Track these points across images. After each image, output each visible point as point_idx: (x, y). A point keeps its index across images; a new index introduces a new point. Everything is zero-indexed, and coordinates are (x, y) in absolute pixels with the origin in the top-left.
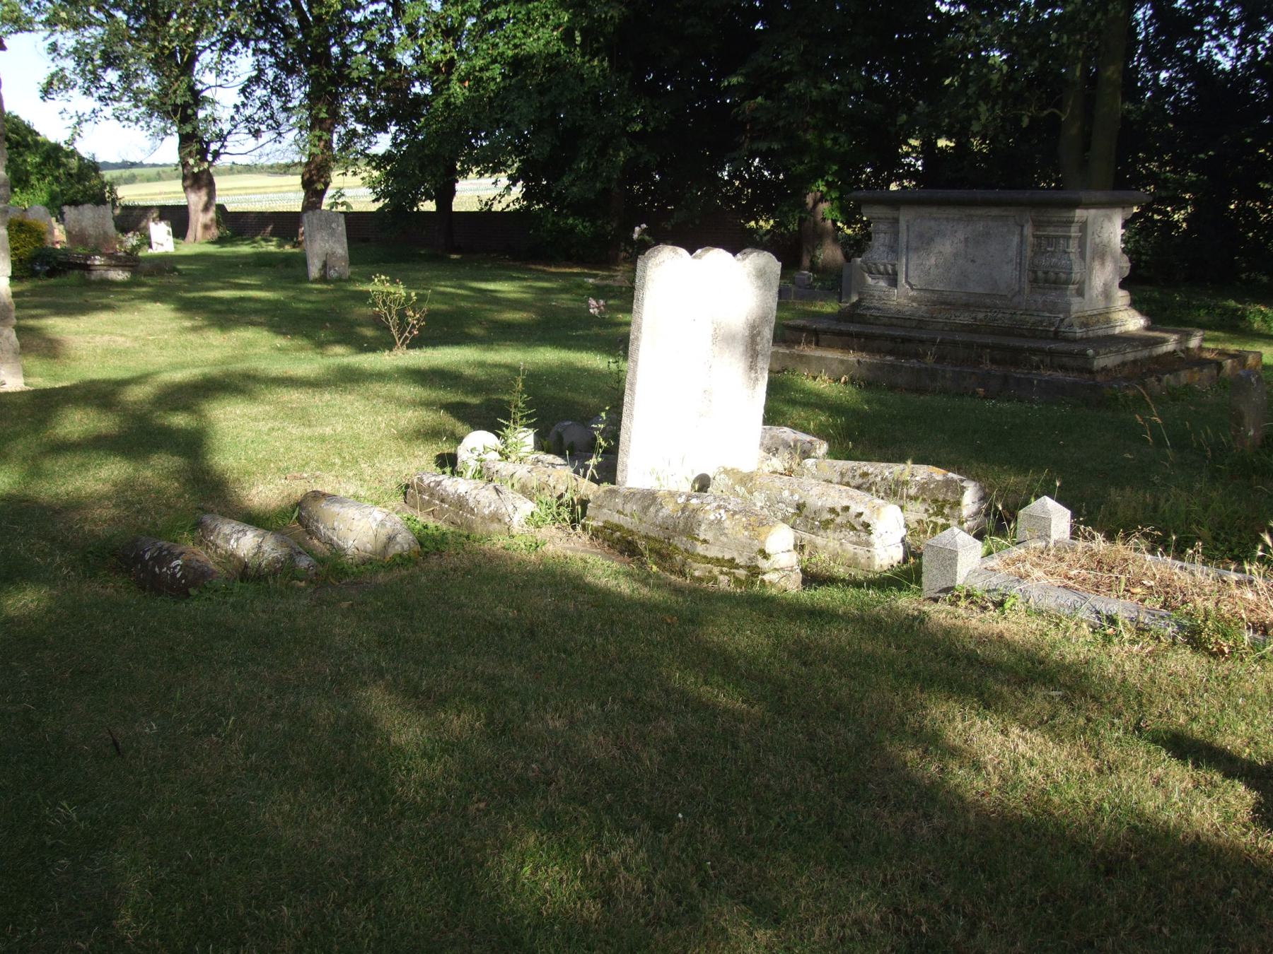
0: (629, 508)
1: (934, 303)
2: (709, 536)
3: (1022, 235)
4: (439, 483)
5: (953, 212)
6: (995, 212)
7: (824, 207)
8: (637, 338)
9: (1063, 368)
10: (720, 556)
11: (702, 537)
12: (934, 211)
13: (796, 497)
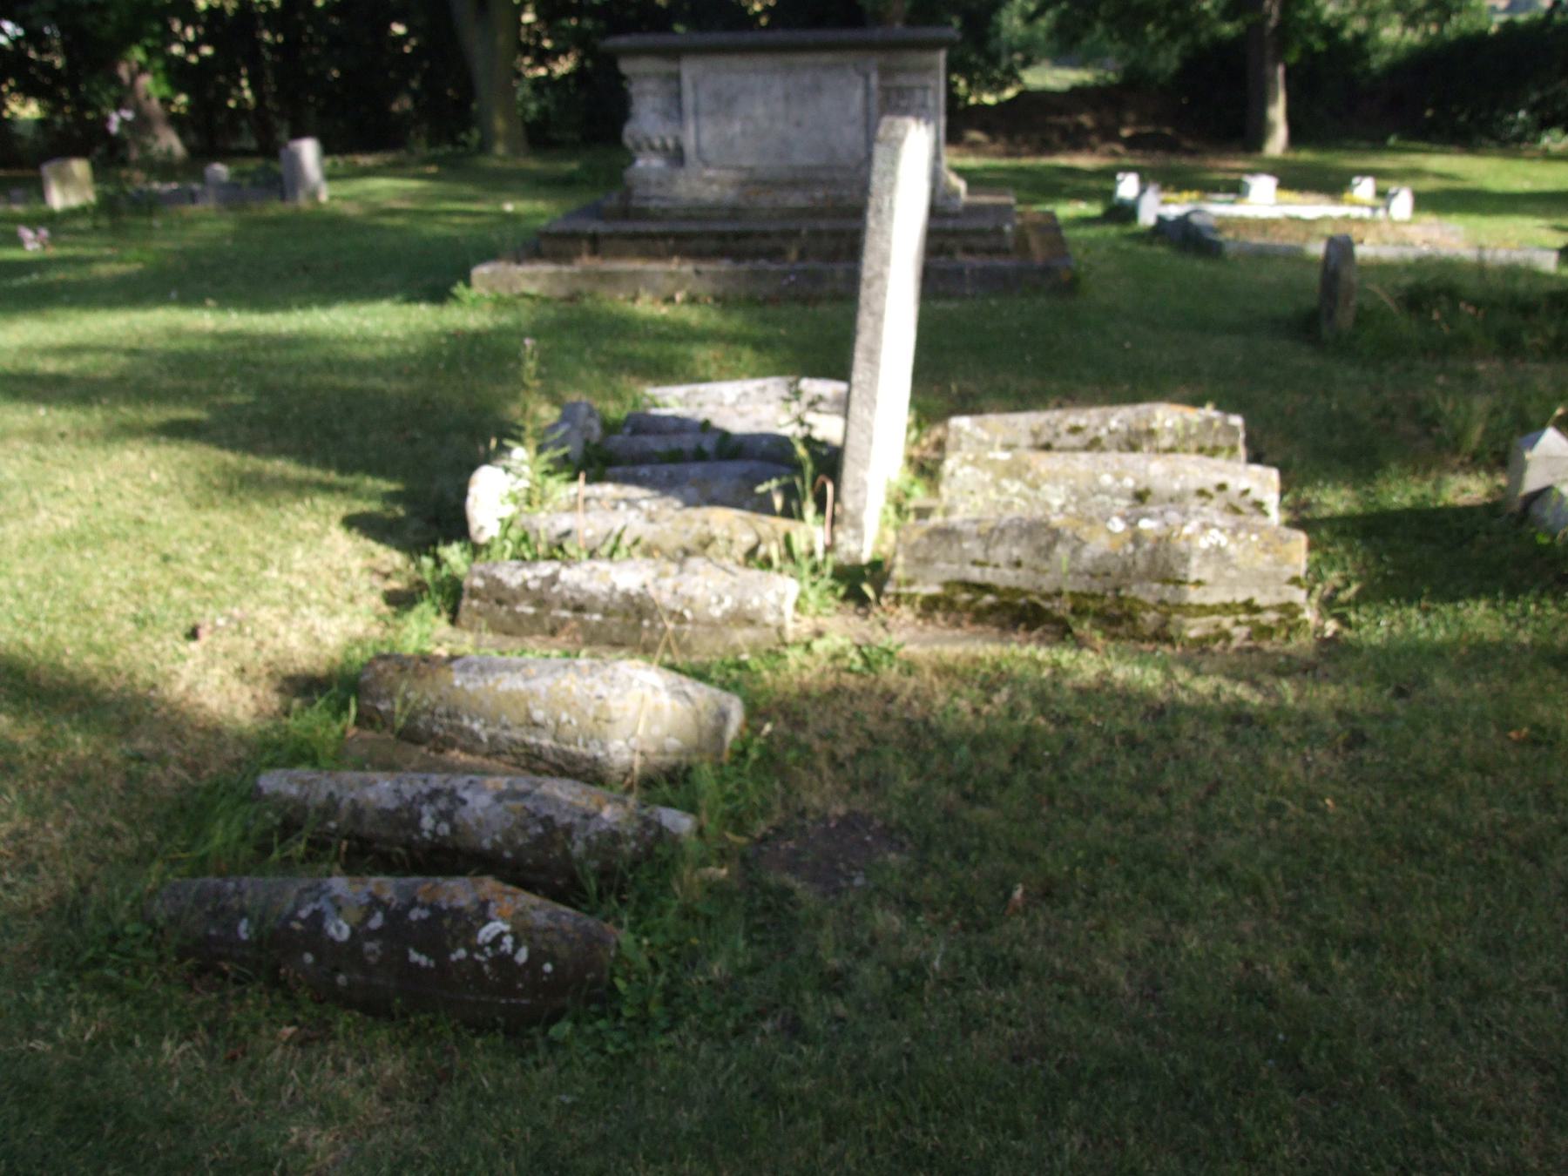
0: (1000, 553)
1: (743, 184)
2: (1207, 574)
3: (867, 88)
4: (553, 579)
5: (764, 61)
6: (827, 58)
7: (146, 81)
8: (881, 276)
9: (969, 250)
10: (1228, 599)
11: (1193, 577)
12: (737, 62)
13: (1129, 483)
